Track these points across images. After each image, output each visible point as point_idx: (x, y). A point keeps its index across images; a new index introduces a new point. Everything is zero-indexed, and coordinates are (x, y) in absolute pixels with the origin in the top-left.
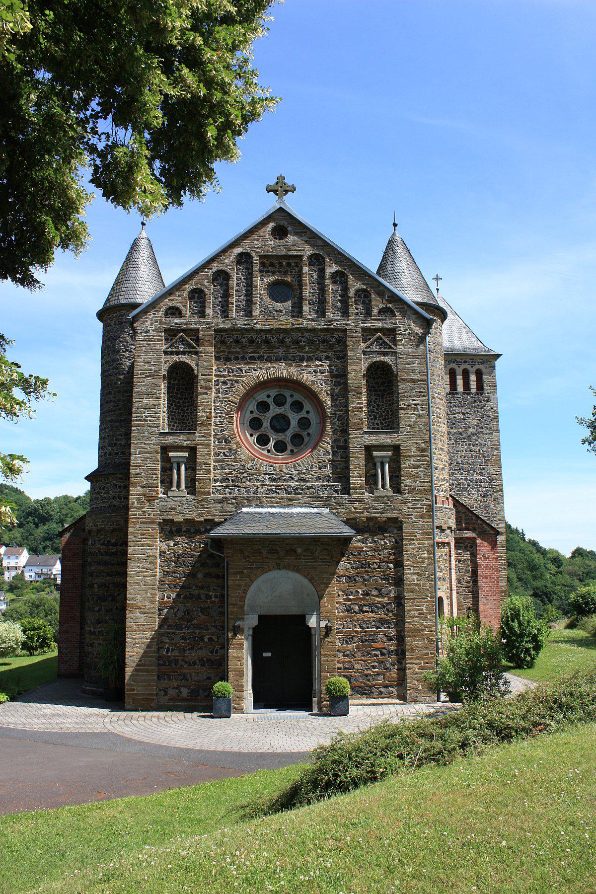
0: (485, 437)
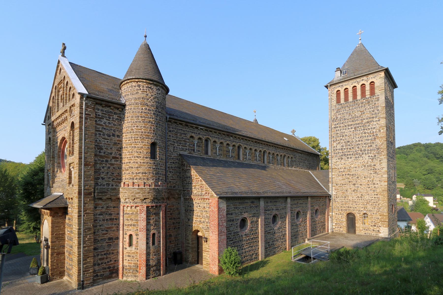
0: (375, 123)
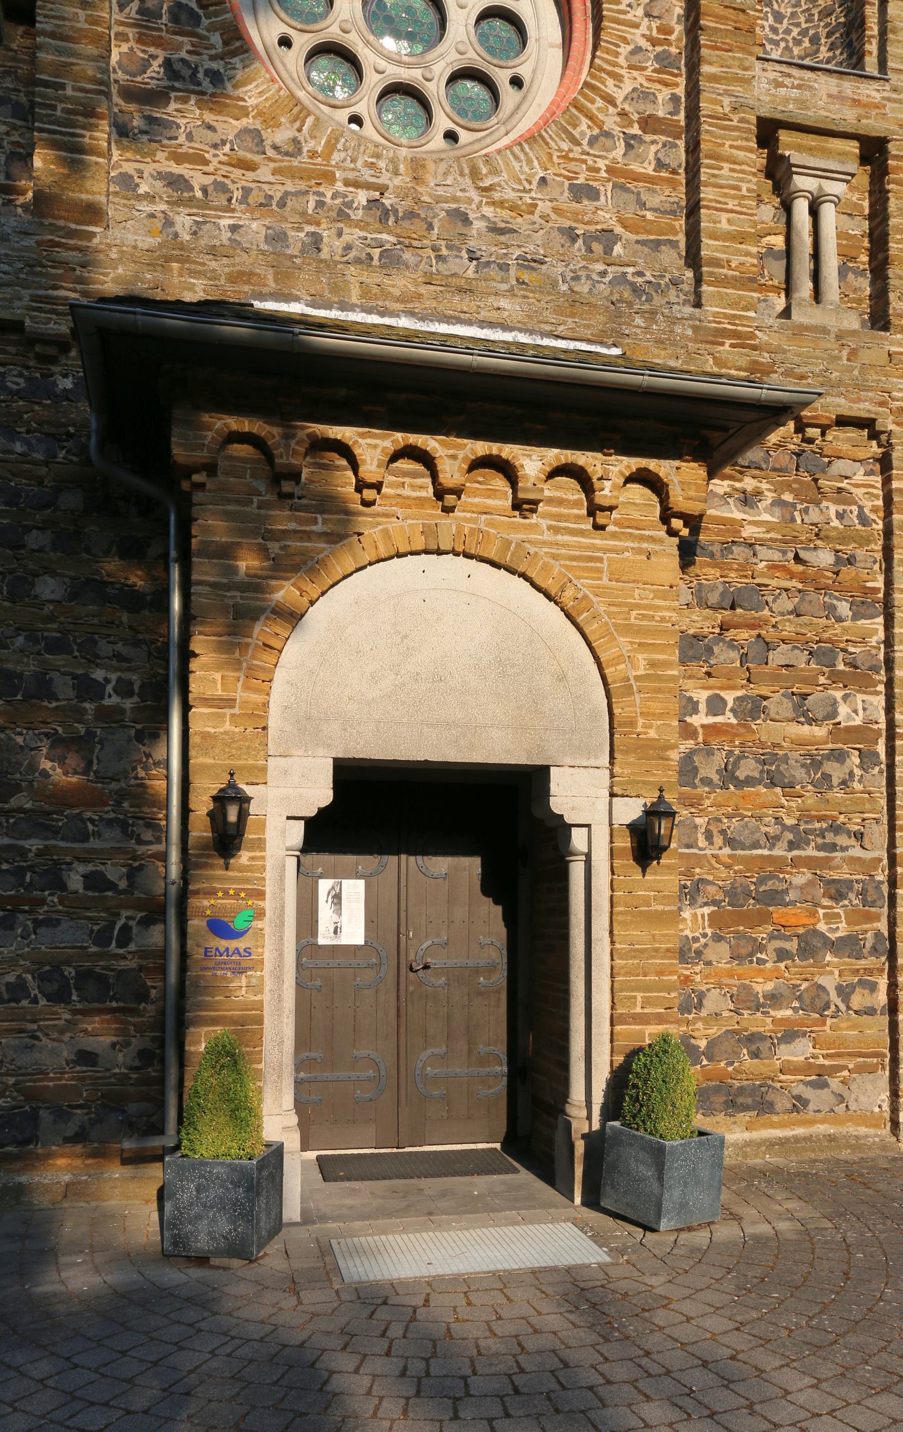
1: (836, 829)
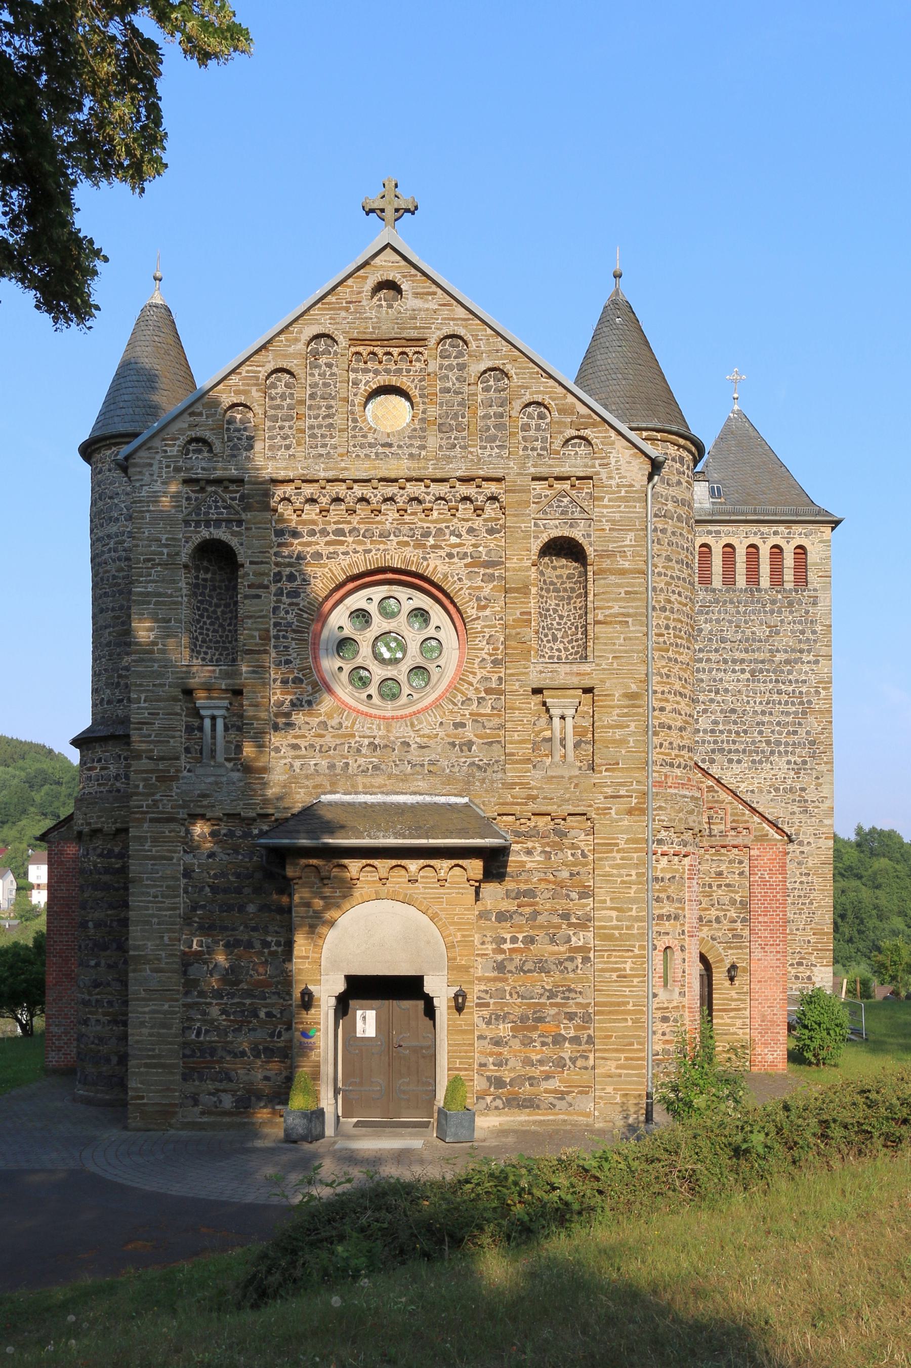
0: (806, 668)
1: (570, 990)
